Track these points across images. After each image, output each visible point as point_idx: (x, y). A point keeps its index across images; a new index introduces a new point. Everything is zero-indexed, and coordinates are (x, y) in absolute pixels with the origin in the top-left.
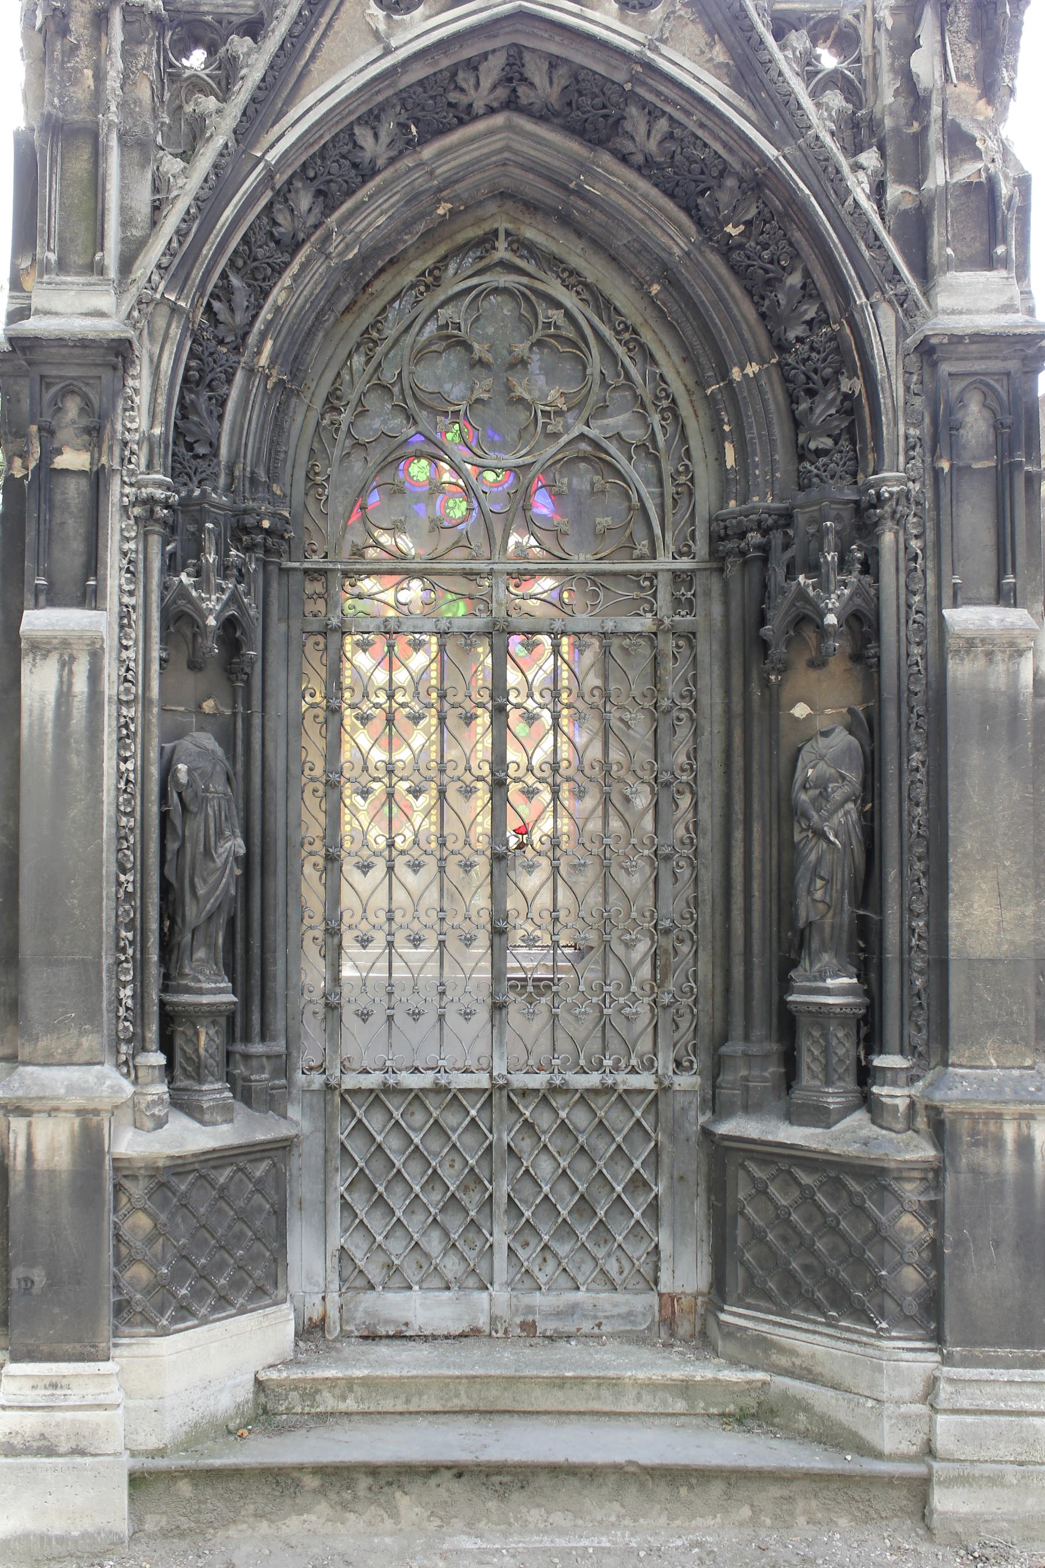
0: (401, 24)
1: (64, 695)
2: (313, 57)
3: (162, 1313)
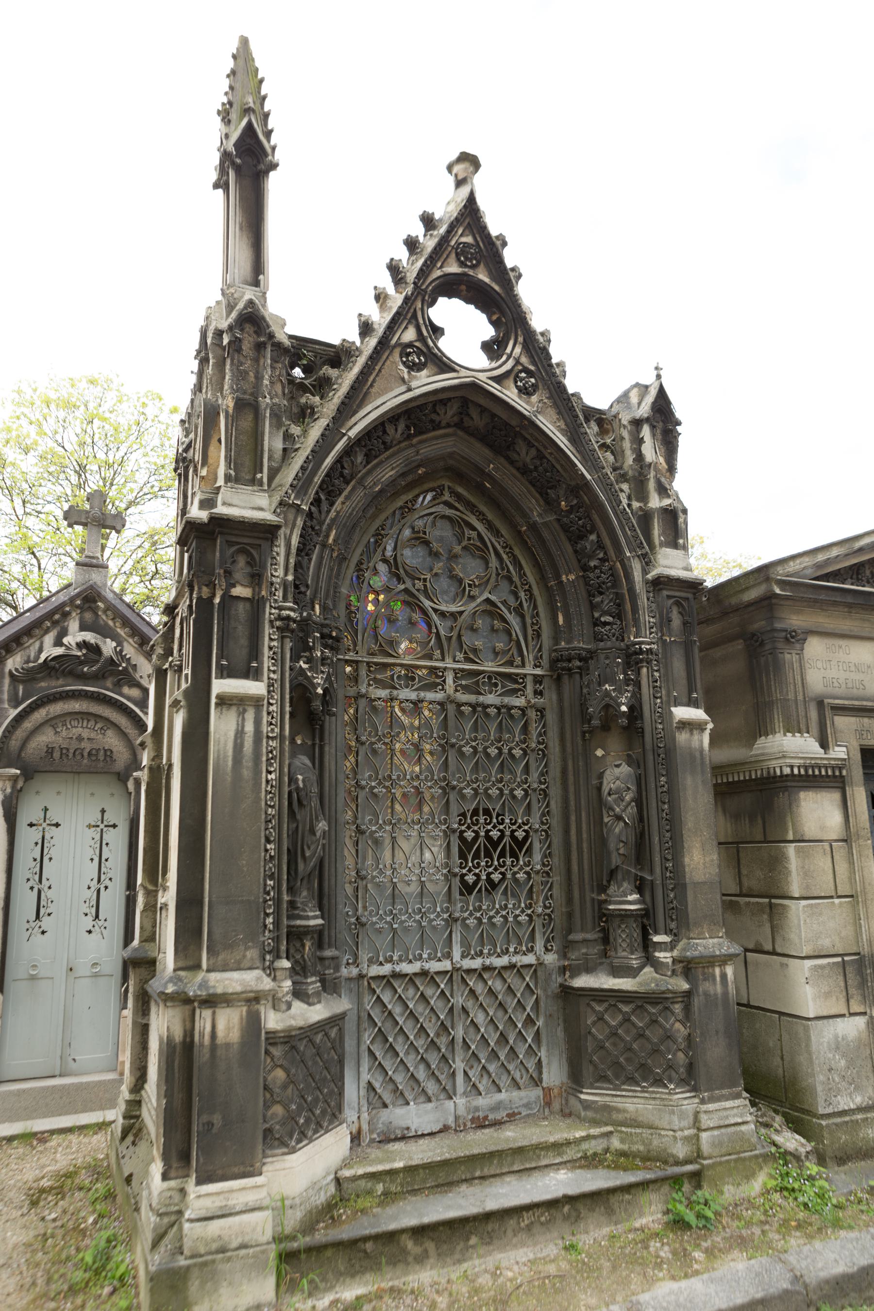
0: (415, 377)
1: (240, 734)
2: (371, 386)
3: (291, 1138)
